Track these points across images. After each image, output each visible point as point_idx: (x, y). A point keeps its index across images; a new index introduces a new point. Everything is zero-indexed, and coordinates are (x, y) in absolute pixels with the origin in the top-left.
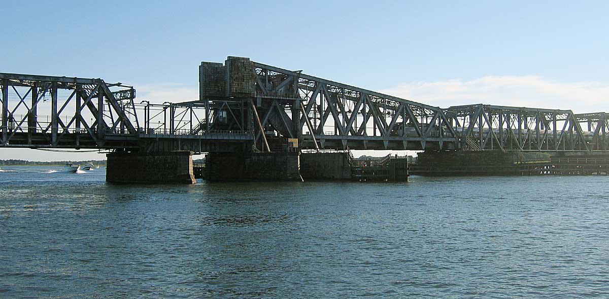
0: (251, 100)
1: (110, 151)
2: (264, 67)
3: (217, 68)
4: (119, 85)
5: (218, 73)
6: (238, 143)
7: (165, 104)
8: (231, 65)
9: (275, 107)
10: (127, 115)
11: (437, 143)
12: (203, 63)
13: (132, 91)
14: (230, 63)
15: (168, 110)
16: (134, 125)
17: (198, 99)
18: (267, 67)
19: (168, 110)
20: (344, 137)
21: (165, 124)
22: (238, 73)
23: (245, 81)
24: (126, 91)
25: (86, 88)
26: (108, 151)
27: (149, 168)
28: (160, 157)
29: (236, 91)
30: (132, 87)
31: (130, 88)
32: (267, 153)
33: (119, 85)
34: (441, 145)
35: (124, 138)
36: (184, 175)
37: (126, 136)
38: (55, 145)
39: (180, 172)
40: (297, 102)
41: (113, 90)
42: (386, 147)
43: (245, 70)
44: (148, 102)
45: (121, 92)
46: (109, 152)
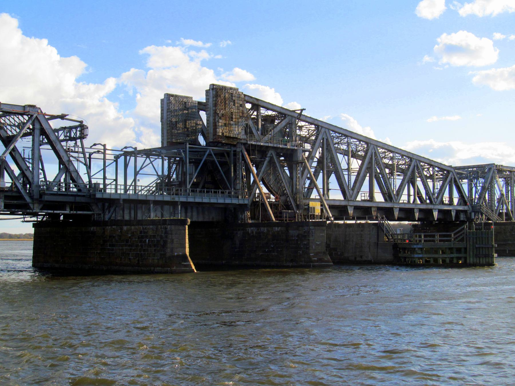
0: (243, 147)
1: (39, 220)
2: (256, 102)
3: (185, 103)
4: (62, 117)
5: (187, 109)
6: (225, 208)
7: (124, 150)
8: (217, 96)
9: (271, 158)
10: (75, 164)
11: (449, 211)
12: (168, 96)
13: (82, 127)
14: (214, 93)
15: (121, 160)
16: (86, 179)
17: (160, 146)
18: (260, 103)
19: (121, 160)
20: (351, 203)
21: (116, 180)
22: (225, 109)
23: (234, 120)
24: (71, 128)
25: (8, 122)
26: (35, 219)
27: (110, 246)
28: (133, 227)
29: (223, 133)
30: (81, 122)
31: (78, 124)
32: (271, 224)
33: (62, 117)
34: (453, 214)
35: (71, 199)
36: (178, 256)
37: (74, 195)
38: (169, 140)
39: (172, 251)
40: (299, 151)
41: (55, 124)
42: (396, 218)
43: (234, 105)
44: (104, 146)
45: (64, 129)
46: (37, 221)
